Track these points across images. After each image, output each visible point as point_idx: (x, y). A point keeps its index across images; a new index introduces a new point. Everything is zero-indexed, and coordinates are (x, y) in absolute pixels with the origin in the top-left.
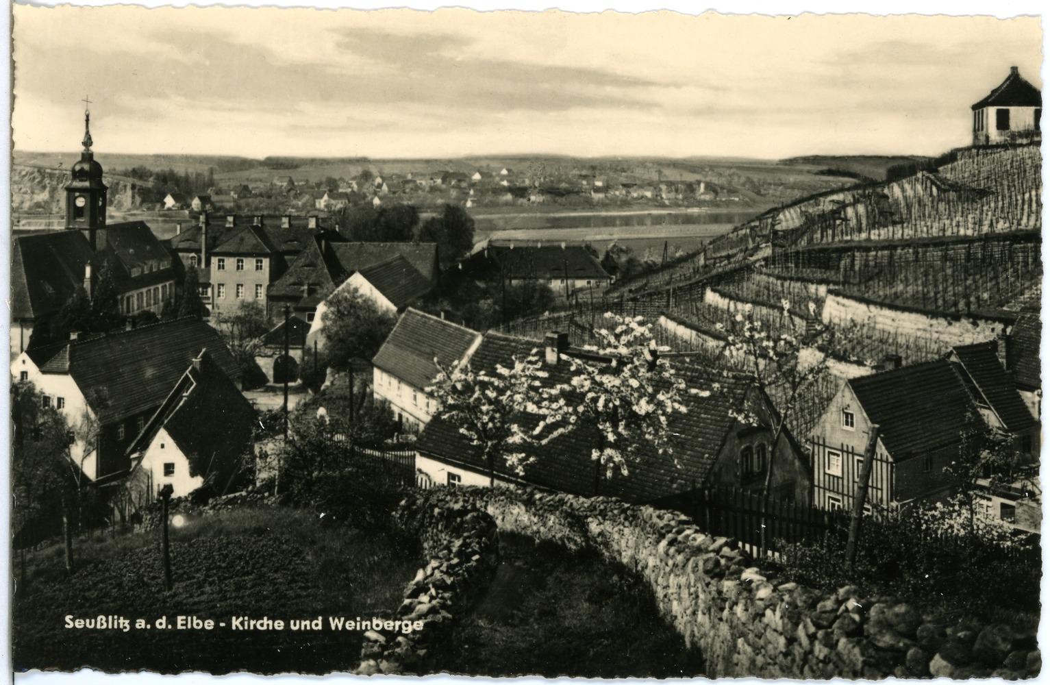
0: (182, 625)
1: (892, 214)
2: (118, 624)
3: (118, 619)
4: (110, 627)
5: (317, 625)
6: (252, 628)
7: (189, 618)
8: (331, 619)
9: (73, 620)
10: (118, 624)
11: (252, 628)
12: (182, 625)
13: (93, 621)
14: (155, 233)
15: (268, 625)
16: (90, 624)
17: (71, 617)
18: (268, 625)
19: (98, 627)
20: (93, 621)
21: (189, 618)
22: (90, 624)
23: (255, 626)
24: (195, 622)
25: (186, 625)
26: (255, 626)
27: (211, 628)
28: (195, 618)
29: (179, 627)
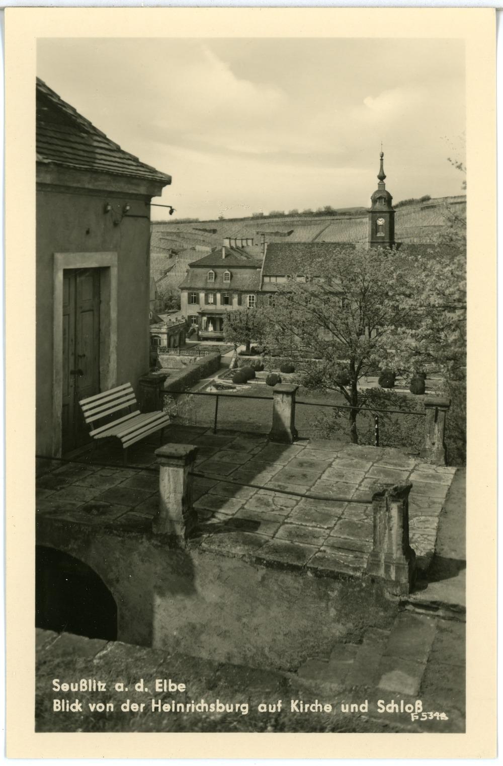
0: (160, 688)
1: (233, 541)
3: (97, 683)
4: (63, 710)
5: (364, 708)
6: (306, 710)
8: (90, 705)
9: (385, 705)
11: (306, 710)
12: (160, 688)
13: (77, 685)
14: (81, 637)
15: (395, 708)
17: (58, 680)
18: (395, 708)
19: (82, 690)
20: (77, 685)
21: (165, 681)
23: (309, 708)
24: (171, 685)
25: (162, 688)
26: (239, 708)
27: (328, 711)
28: (170, 681)
29: (158, 690)
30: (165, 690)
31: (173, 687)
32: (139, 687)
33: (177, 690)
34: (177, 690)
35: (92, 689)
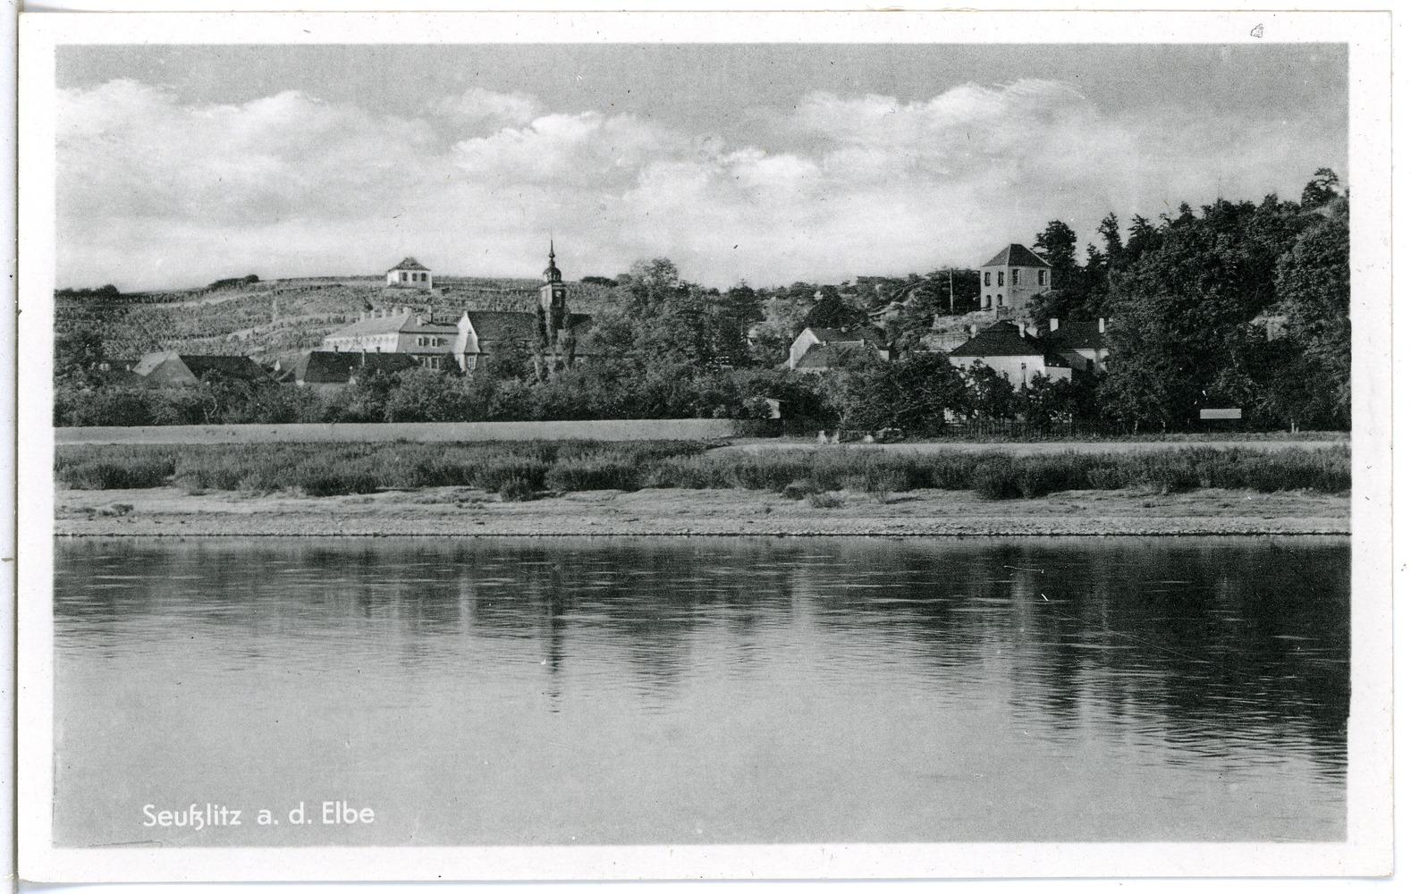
2: (220, 816)
7: (338, 803)
10: (220, 816)
16: (181, 820)
21: (338, 803)
22: (181, 820)
24: (346, 811)
30: (338, 821)
31: (350, 816)
32: (296, 817)
33: (359, 820)
34: (158, 824)
35: (213, 819)
